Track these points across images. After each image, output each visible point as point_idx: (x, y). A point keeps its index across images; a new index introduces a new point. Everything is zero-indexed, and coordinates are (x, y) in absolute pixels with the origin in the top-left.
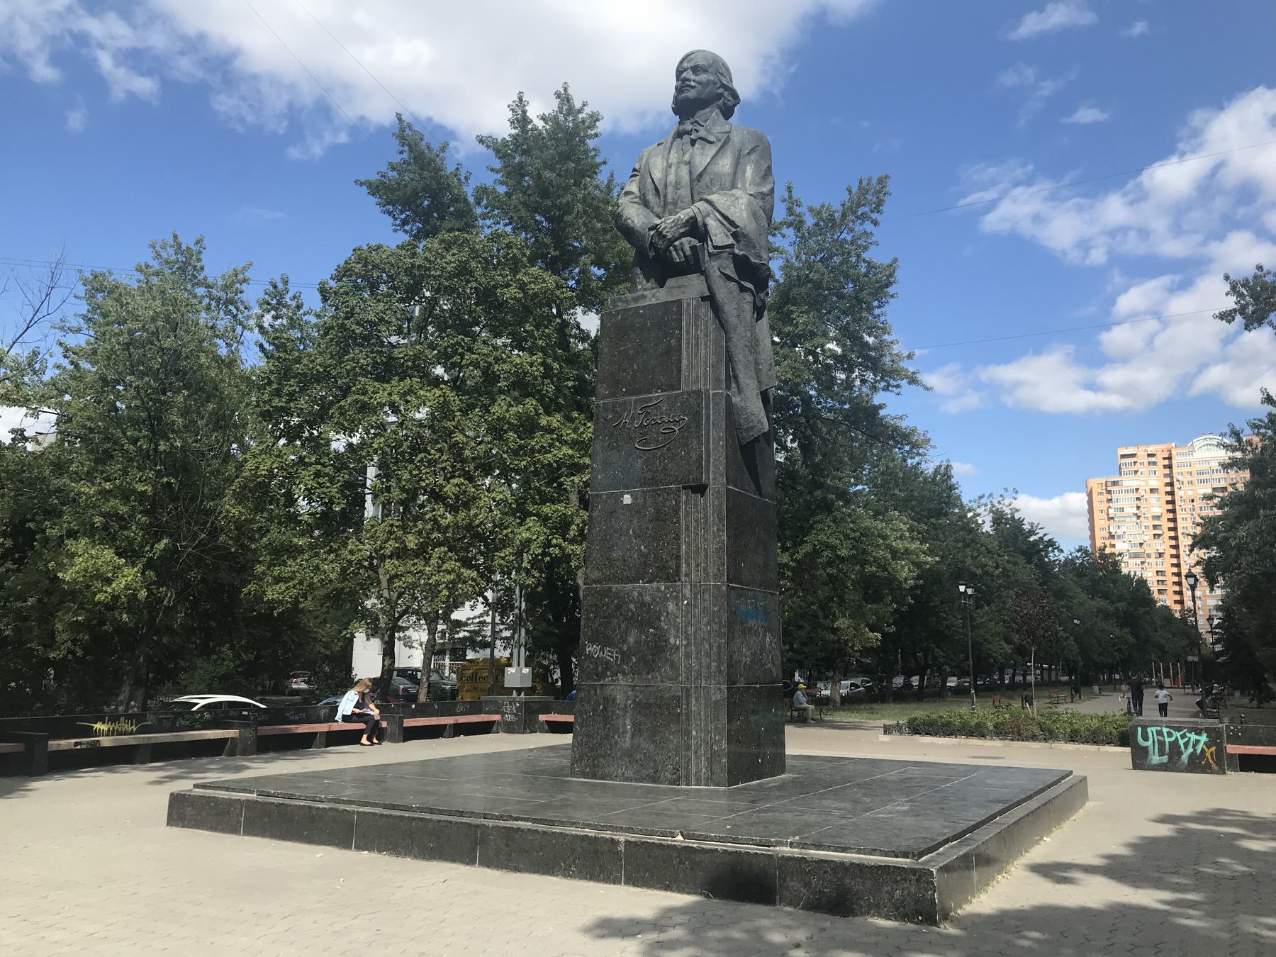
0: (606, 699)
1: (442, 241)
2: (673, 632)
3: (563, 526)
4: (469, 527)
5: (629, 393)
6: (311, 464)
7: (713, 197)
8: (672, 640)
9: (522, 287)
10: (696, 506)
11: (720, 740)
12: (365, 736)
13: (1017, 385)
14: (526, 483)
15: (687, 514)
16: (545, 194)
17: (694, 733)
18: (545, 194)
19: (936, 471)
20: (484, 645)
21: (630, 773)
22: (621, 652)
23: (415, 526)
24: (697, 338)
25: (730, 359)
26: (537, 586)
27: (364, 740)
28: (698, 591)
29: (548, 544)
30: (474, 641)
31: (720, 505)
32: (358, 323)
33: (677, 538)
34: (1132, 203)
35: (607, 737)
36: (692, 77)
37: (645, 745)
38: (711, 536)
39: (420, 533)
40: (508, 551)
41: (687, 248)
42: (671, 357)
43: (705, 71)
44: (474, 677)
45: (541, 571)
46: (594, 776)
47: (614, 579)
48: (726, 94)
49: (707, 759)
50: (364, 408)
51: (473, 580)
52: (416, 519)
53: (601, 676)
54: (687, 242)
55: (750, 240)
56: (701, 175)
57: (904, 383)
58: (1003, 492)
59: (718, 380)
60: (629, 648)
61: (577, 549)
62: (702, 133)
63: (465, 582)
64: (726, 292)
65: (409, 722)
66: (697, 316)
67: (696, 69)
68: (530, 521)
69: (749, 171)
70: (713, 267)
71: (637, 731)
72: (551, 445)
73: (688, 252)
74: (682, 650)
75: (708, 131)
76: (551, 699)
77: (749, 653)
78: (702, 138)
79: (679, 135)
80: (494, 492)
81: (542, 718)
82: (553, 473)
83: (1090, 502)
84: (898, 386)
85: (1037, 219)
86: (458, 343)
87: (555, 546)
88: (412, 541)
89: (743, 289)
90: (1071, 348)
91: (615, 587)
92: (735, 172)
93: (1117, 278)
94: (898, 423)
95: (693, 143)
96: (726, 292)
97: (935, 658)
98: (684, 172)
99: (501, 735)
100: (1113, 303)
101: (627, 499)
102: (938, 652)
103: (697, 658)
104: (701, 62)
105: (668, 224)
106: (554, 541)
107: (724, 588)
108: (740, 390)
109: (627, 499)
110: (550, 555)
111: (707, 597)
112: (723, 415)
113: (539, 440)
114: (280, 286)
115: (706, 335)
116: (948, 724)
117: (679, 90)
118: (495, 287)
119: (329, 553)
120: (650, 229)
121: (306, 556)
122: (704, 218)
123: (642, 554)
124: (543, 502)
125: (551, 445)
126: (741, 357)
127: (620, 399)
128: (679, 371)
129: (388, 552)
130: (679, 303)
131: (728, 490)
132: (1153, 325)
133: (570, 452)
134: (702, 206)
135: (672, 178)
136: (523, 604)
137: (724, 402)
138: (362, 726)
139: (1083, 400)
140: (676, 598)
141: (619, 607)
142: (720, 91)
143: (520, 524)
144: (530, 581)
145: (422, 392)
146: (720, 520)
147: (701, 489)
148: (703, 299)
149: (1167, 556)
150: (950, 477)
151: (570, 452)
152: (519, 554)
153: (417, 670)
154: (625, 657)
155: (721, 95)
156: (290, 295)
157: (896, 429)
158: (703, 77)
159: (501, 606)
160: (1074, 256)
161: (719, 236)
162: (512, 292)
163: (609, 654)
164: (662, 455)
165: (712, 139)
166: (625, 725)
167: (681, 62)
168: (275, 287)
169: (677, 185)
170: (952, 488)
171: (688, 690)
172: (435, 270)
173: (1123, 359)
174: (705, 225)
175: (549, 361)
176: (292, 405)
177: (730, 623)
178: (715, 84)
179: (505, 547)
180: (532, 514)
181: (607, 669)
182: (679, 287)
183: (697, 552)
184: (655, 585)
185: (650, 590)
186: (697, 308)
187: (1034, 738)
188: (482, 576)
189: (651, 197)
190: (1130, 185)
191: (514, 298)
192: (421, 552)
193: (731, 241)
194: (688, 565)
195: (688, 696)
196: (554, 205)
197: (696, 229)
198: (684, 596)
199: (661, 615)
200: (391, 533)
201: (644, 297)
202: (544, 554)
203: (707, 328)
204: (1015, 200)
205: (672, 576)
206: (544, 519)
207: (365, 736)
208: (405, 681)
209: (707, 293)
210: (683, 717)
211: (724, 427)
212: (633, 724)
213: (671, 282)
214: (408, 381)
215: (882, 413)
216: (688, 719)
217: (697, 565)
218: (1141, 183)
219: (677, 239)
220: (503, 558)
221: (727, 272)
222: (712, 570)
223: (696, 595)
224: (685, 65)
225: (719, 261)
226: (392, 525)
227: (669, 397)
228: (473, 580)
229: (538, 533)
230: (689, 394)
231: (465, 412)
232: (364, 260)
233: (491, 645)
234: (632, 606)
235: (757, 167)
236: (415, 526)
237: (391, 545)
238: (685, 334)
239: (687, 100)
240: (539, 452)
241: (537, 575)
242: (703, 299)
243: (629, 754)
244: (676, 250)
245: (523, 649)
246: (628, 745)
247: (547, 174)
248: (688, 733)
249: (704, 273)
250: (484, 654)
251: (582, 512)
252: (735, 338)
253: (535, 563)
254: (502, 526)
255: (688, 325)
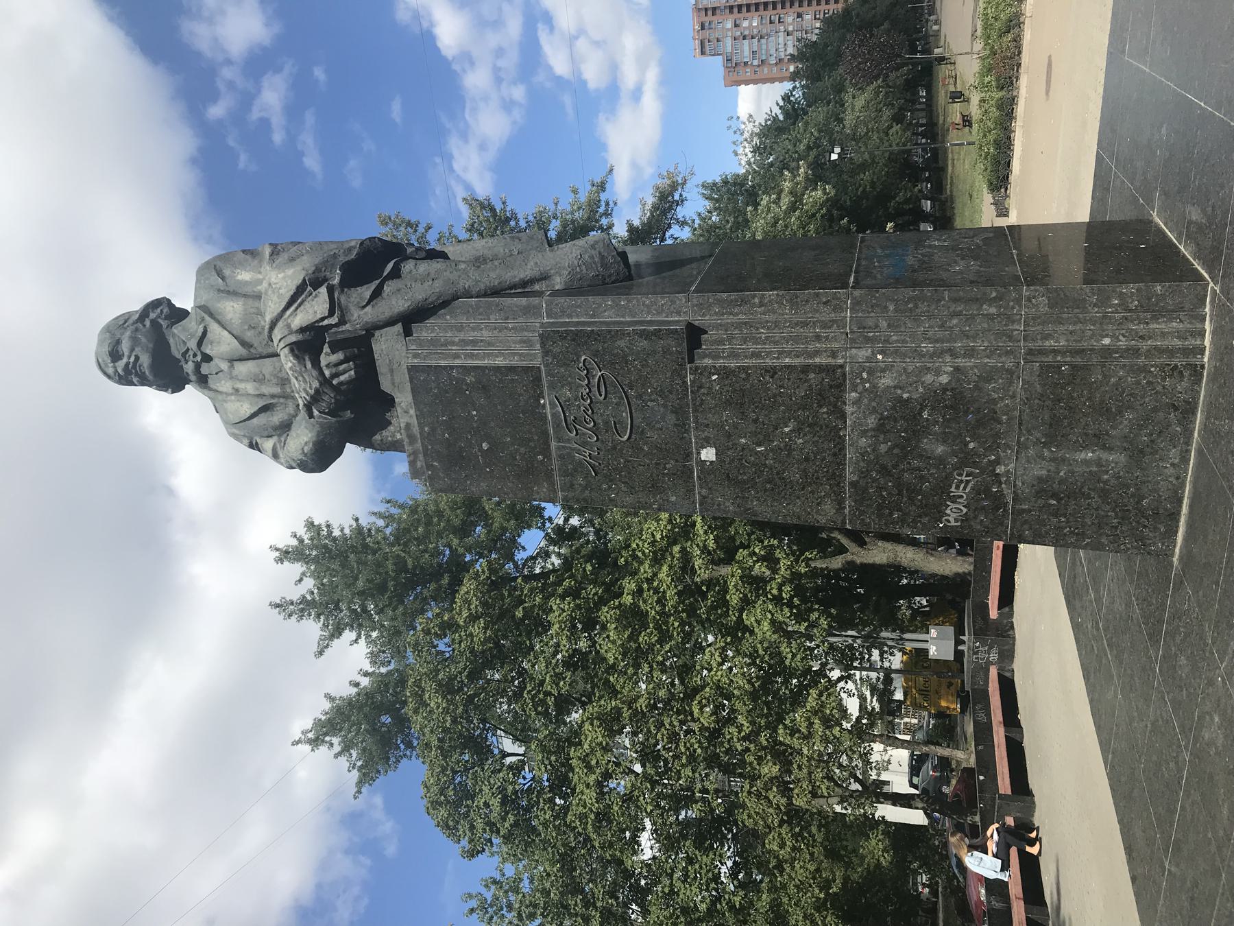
0: (1039, 493)
1: (416, 711)
2: (929, 378)
3: (757, 584)
4: (754, 696)
5: (546, 451)
6: (672, 885)
7: (268, 318)
8: (944, 379)
9: (473, 618)
10: (721, 342)
11: (1121, 296)
12: (1028, 849)
13: (634, 165)
14: (706, 624)
15: (733, 355)
16: (382, 588)
17: (1107, 341)
18: (382, 588)
19: (708, 198)
20: (888, 680)
21: (1174, 454)
22: (959, 467)
23: (751, 764)
24: (464, 342)
25: (497, 292)
26: (829, 615)
27: (1034, 850)
28: (862, 336)
29: (778, 600)
30: (884, 694)
31: (720, 302)
32: (504, 819)
33: (772, 371)
34: (472, 63)
35: (1104, 494)
36: (125, 360)
37: (1123, 427)
38: (771, 317)
39: (760, 759)
40: (784, 649)
41: (334, 358)
42: (488, 381)
43: (118, 342)
44: (924, 693)
45: (811, 610)
46: (1174, 516)
47: (836, 478)
48: (152, 316)
49: (1155, 318)
50: (603, 817)
51: (820, 695)
52: (743, 763)
53: (998, 501)
54: (327, 358)
55: (325, 262)
56: (243, 343)
57: (603, 197)
58: (731, 131)
59: (527, 310)
60: (954, 453)
61: (784, 563)
62: (192, 344)
63: (823, 706)
64: (397, 299)
65: (1004, 785)
66: (433, 342)
67: (115, 355)
68: (749, 620)
69: (244, 276)
70: (360, 315)
71: (1098, 440)
72: (656, 591)
73: (340, 356)
74: (961, 362)
75: (192, 336)
76: (968, 605)
77: (962, 263)
78: (200, 344)
79: (203, 381)
80: (722, 666)
81: (994, 614)
82: (691, 592)
83: (747, 82)
84: (607, 204)
85: (482, 147)
86: (532, 699)
87: (780, 590)
88: (770, 769)
89: (396, 274)
90: (602, 116)
91: (850, 475)
92: (245, 296)
93: (540, 77)
94: (648, 207)
95: (207, 358)
96: (397, 299)
97: (907, 201)
98: (243, 368)
99: (1015, 666)
100: (560, 78)
101: (708, 454)
102: (900, 197)
103: (974, 338)
104: (106, 349)
105: (302, 386)
106: (775, 592)
107: (857, 293)
108: (544, 277)
109: (708, 454)
110: (792, 597)
111: (870, 322)
112: (580, 300)
113: (650, 606)
114: (474, 903)
115: (460, 329)
116: (997, 143)
117: (144, 381)
118: (472, 651)
119: (782, 871)
120: (311, 416)
121: (785, 900)
122: (291, 333)
123: (798, 431)
124: (726, 603)
125: (656, 591)
126: (492, 277)
127: (555, 466)
128: (511, 369)
129: (784, 801)
130: (412, 370)
131: (696, 291)
132: (582, 45)
133: (665, 568)
134: (277, 334)
135: (250, 388)
136: (850, 633)
137: (561, 300)
138: (1014, 852)
139: (650, 104)
140: (871, 372)
141: (884, 470)
142: (148, 323)
143: (752, 632)
144: (824, 623)
145: (586, 746)
146: (744, 302)
147: (694, 335)
148: (408, 333)
149: (800, 10)
150: (715, 184)
151: (665, 568)
152: (789, 636)
153: (912, 755)
154: (967, 459)
155: (154, 322)
156: (483, 891)
157: (655, 207)
158: (125, 347)
159: (847, 659)
160: (517, 114)
161: (316, 308)
162: (477, 630)
163: (962, 488)
164: (640, 396)
165: (201, 329)
166: (1086, 462)
167: (109, 377)
168: (472, 911)
169: (259, 379)
170: (725, 182)
171: (1030, 352)
172: (445, 721)
173: (614, 68)
174: (302, 330)
175: (560, 590)
176: (599, 904)
177: (915, 284)
178: (137, 330)
179: (780, 653)
180: (740, 617)
181: (987, 491)
182: (392, 371)
183: (796, 339)
184: (849, 409)
185: (855, 411)
186: (420, 343)
187: (1017, 41)
188: (815, 683)
189: (277, 418)
190: (456, 67)
191: (485, 628)
192: (783, 756)
193: (323, 290)
194: (817, 353)
195: (1042, 352)
196: (394, 579)
197: (309, 344)
198: (869, 359)
199: (900, 400)
200: (759, 795)
201: (408, 426)
202: (790, 605)
203: (451, 328)
204: (465, 169)
205: (832, 384)
206: (746, 603)
207: (1028, 849)
208: (924, 768)
209: (399, 328)
210: (1078, 360)
211: (598, 299)
212: (1086, 447)
213: (386, 385)
214: (574, 762)
215: (636, 223)
216: (1081, 352)
217: (818, 338)
218: (454, 58)
219: (321, 373)
220: (794, 656)
221: (368, 294)
222: (826, 314)
223: (868, 340)
224: (110, 371)
225: (352, 308)
226: (750, 793)
227: (552, 386)
228: (820, 695)
229: (765, 611)
230: (546, 353)
231: (614, 693)
232: (435, 804)
233: (888, 673)
234: (883, 448)
235: (242, 265)
236: (751, 764)
237: (773, 794)
238: (458, 362)
239: (153, 366)
240: (664, 606)
241: (816, 614)
242: (408, 333)
243: (1138, 454)
244: (337, 375)
245: (906, 636)
246: (1122, 458)
247: (360, 584)
248: (1107, 352)
249: (371, 330)
250: (899, 683)
251: (739, 557)
252: (464, 283)
253: (799, 617)
254: (753, 655)
255: (445, 356)
